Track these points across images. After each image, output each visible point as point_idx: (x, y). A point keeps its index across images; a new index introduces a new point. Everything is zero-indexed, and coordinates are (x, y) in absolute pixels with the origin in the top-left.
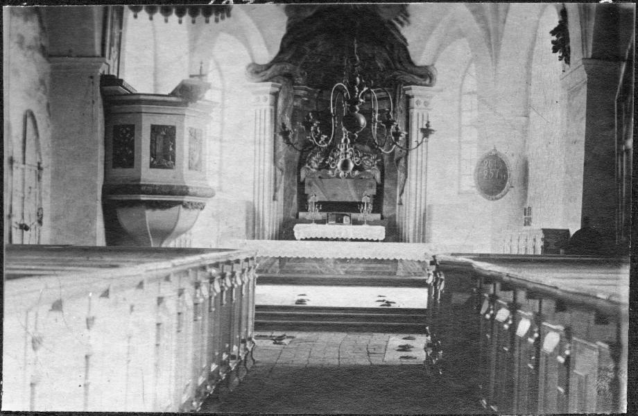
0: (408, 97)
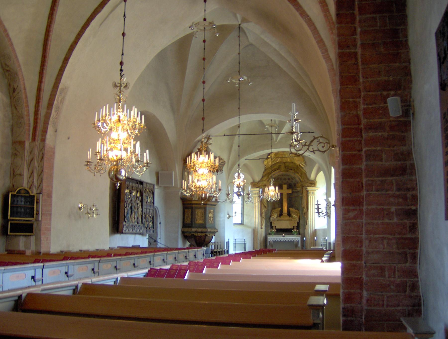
0: (307, 191)
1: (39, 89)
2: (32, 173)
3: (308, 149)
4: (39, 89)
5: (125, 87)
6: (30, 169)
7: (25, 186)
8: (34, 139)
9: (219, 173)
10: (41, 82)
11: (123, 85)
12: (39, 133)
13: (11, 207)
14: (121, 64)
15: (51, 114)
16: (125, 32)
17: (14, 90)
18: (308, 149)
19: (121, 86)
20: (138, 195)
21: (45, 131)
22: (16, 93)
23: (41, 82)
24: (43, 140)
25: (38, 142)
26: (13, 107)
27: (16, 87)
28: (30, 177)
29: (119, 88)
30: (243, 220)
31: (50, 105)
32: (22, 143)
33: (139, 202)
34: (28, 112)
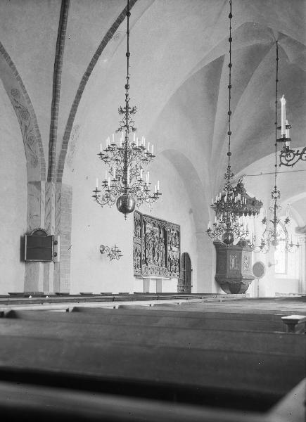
1: (53, 127)
2: (49, 214)
3: (301, 158)
4: (53, 127)
5: (132, 112)
6: (47, 210)
7: (43, 227)
8: (49, 180)
9: (252, 215)
10: (53, 118)
11: (130, 110)
12: (55, 170)
13: (27, 248)
14: (127, 87)
15: (66, 152)
16: (130, 52)
17: (26, 128)
18: (301, 158)
19: (127, 111)
20: (162, 236)
21: (60, 171)
22: (28, 131)
23: (53, 118)
24: (59, 181)
25: (53, 184)
26: (27, 146)
27: (27, 125)
28: (47, 218)
29: (124, 115)
30: (286, 270)
31: (65, 143)
32: (38, 184)
33: (162, 244)
34: (41, 150)
